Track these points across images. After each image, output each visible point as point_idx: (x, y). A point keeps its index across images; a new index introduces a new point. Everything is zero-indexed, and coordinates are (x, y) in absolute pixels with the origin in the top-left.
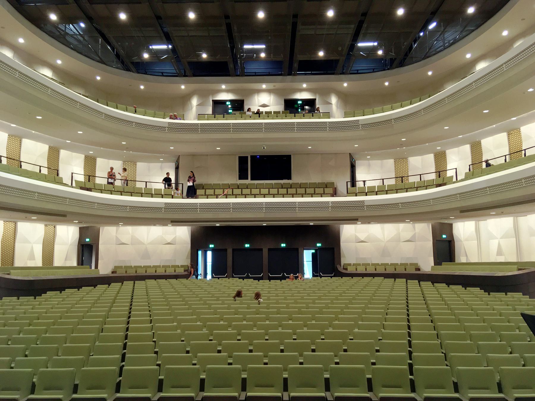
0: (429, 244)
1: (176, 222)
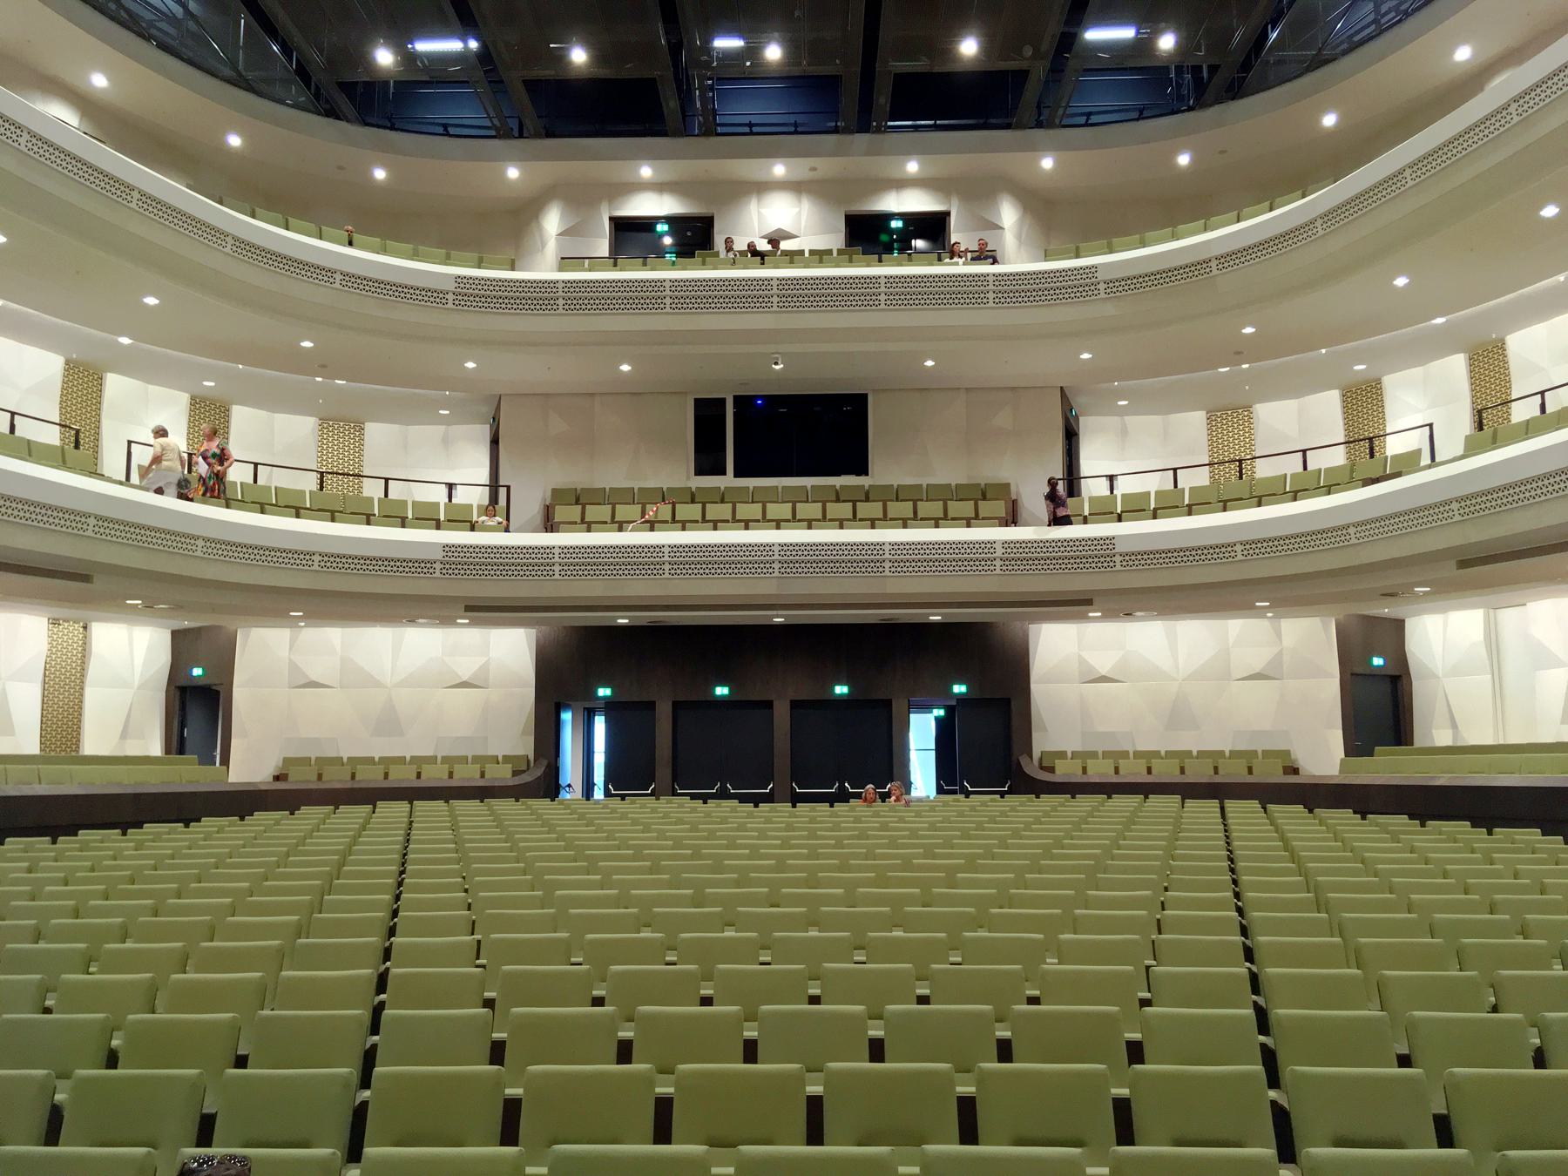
0: (1329, 689)
1: (485, 611)
